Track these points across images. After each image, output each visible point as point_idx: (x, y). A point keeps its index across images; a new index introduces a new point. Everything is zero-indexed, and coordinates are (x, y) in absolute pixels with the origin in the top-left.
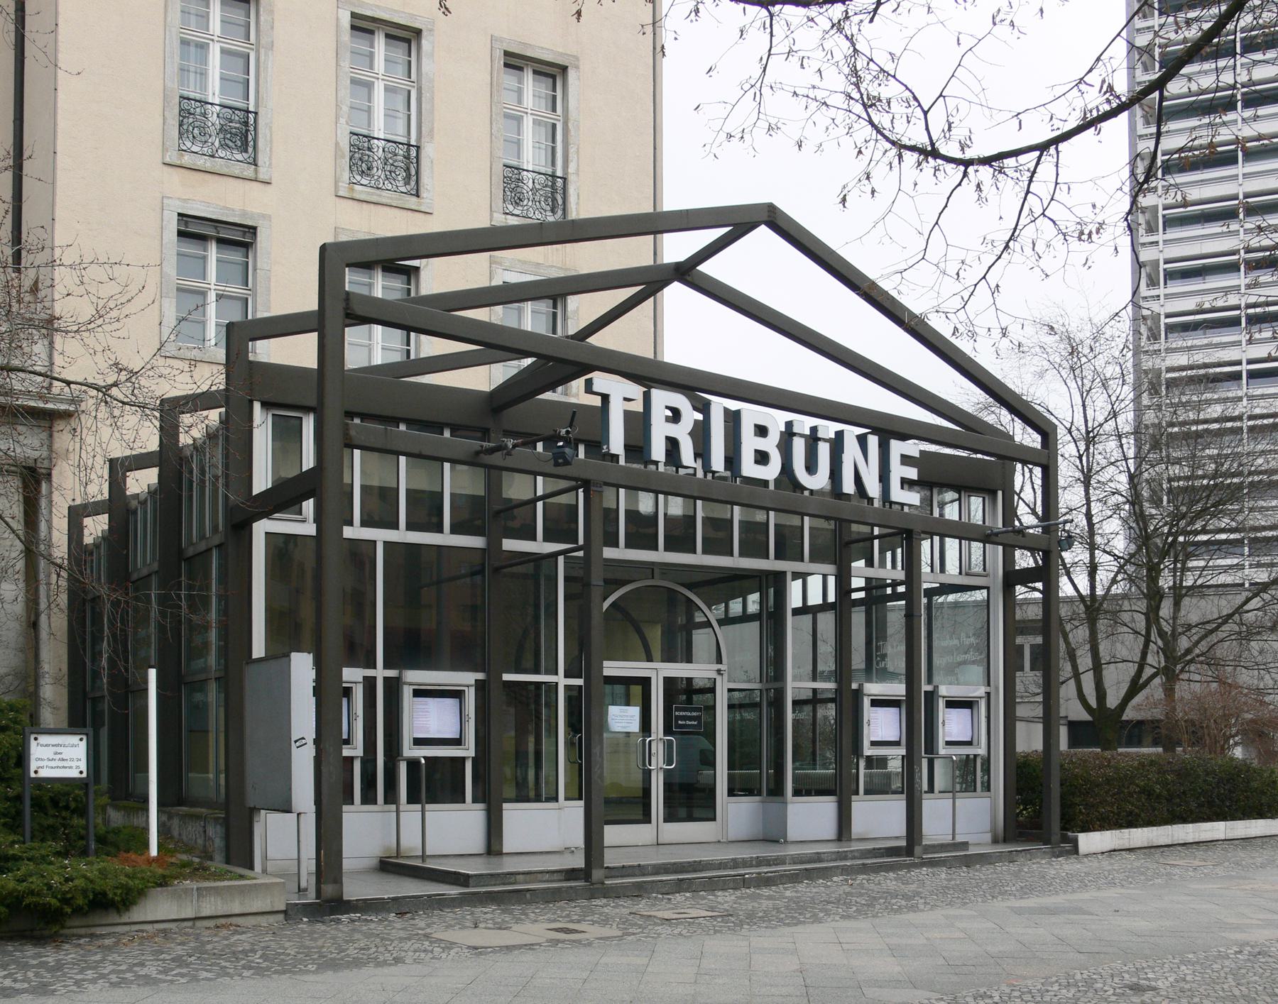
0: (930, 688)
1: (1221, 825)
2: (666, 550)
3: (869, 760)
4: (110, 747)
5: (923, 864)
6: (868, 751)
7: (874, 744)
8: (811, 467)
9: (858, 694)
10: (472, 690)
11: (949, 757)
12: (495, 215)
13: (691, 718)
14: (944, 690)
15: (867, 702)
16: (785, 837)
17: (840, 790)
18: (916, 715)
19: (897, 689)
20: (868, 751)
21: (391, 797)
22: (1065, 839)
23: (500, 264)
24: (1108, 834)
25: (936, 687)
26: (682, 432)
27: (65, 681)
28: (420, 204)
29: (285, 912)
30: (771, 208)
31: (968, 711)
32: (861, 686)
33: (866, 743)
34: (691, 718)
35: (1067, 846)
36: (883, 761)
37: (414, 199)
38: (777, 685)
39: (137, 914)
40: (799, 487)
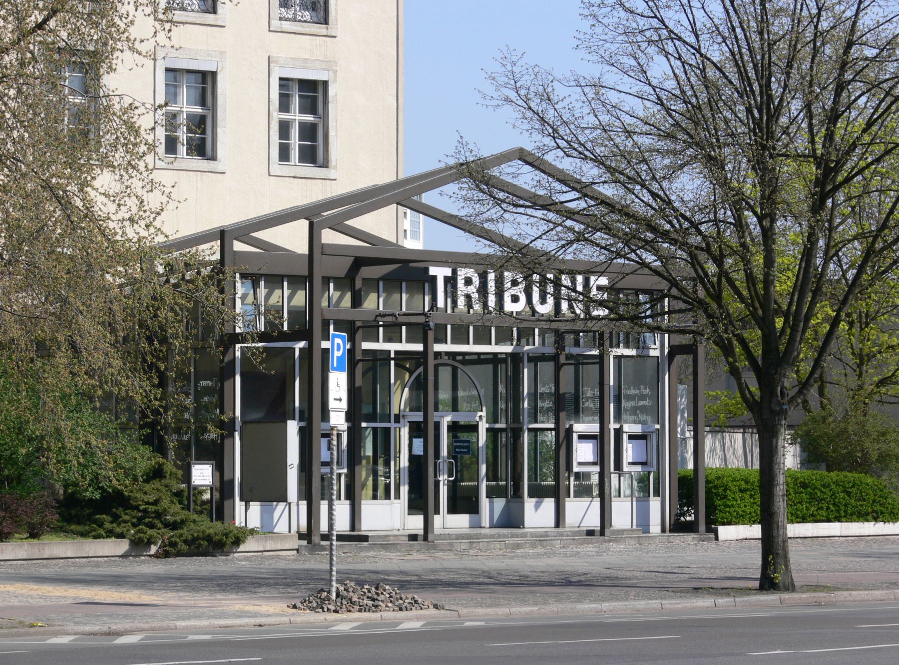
0: (617, 426)
1: (837, 525)
2: (452, 343)
3: (578, 476)
4: (861, 516)
5: (610, 541)
6: (576, 469)
7: (580, 464)
8: (543, 301)
9: (569, 431)
10: (346, 433)
11: (630, 473)
12: (272, 22)
13: (463, 447)
14: (627, 428)
15: (575, 436)
16: (523, 525)
17: (557, 493)
18: (606, 448)
19: (593, 428)
20: (576, 469)
21: (387, 496)
22: (709, 530)
23: (277, 62)
24: (741, 527)
25: (621, 427)
26: (472, 289)
27: (775, 526)
28: (217, 20)
29: (297, 550)
30: (521, 150)
31: (644, 442)
32: (571, 426)
33: (575, 464)
34: (463, 447)
35: (712, 536)
36: (587, 475)
37: (212, 16)
38: (443, 355)
39: (242, 548)
40: (534, 312)
